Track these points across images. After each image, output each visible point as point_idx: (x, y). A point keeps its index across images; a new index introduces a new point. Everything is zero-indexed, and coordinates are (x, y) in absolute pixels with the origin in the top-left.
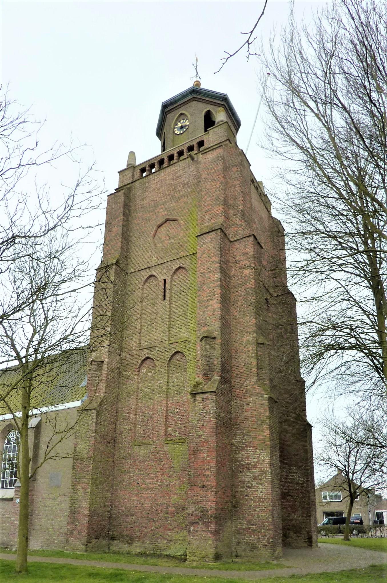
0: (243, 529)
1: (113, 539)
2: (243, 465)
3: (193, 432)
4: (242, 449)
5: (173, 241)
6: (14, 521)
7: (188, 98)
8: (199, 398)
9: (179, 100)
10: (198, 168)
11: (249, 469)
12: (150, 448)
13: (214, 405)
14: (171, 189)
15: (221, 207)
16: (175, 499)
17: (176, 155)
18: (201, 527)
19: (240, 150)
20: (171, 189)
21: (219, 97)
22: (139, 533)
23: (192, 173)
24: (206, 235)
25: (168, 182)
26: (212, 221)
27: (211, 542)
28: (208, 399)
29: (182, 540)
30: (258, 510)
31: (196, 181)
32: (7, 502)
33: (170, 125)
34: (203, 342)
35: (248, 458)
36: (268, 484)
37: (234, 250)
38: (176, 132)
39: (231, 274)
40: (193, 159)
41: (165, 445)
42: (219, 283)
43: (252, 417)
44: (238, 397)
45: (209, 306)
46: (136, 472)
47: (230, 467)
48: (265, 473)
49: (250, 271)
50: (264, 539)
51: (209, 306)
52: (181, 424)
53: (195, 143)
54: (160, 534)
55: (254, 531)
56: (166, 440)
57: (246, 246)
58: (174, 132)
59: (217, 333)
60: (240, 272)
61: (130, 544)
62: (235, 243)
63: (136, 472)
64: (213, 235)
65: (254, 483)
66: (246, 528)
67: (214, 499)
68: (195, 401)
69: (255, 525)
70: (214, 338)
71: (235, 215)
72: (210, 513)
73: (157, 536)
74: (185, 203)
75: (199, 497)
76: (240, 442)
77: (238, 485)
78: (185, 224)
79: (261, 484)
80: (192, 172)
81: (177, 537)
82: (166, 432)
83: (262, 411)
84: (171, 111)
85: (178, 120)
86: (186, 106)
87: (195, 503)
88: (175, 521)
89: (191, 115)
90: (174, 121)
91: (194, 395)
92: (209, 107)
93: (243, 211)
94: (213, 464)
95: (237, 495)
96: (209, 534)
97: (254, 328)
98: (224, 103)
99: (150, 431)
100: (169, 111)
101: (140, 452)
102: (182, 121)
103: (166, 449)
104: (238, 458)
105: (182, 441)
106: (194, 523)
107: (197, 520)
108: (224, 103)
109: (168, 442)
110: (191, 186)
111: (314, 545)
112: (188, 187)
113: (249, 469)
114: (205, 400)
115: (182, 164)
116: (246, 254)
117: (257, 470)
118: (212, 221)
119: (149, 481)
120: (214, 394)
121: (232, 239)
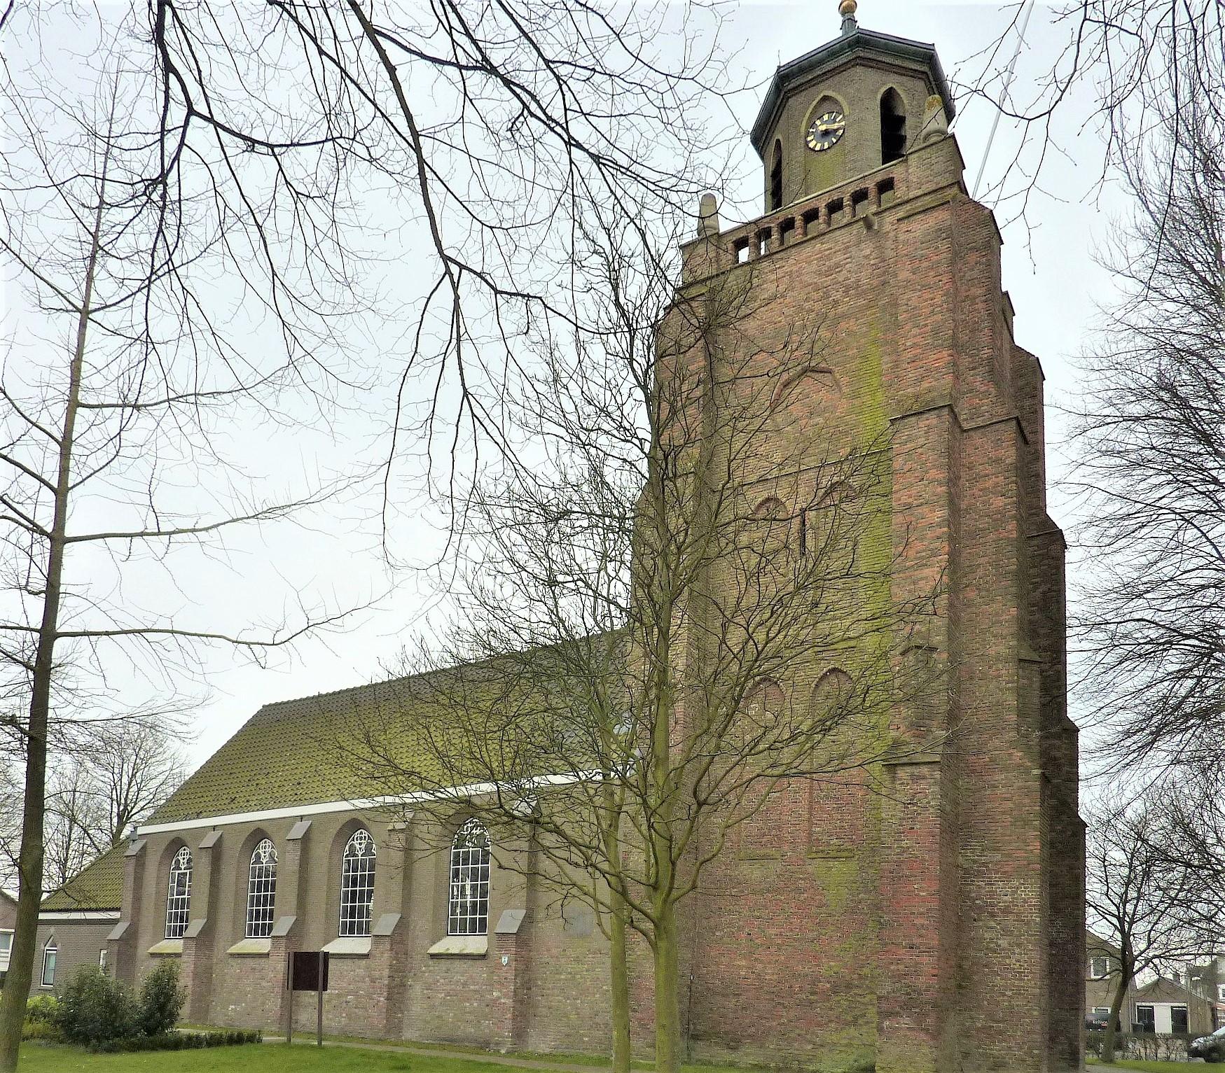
0: (978, 1030)
1: (695, 1037)
2: (980, 908)
3: (889, 841)
4: (979, 874)
5: (821, 420)
6: (499, 998)
7: (843, 59)
8: (903, 773)
9: (821, 62)
10: (880, 248)
11: (993, 915)
12: (776, 867)
13: (937, 789)
14: (815, 296)
15: (945, 353)
16: (830, 967)
17: (823, 211)
18: (905, 1021)
19: (986, 212)
20: (815, 296)
21: (915, 54)
22: (753, 1029)
23: (866, 262)
24: (913, 419)
25: (806, 278)
26: (925, 385)
27: (926, 1050)
28: (924, 778)
29: (846, 1046)
30: (1009, 993)
31: (875, 282)
32: (470, 962)
33: (798, 127)
34: (911, 657)
35: (992, 894)
36: (1034, 945)
37: (970, 450)
38: (811, 145)
39: (963, 506)
40: (869, 226)
41: (809, 861)
42: (946, 529)
43: (1004, 813)
44: (973, 771)
45: (922, 579)
46: (745, 912)
47: (961, 912)
48: (1028, 923)
49: (1007, 501)
50: (1021, 1048)
51: (922, 579)
52: (842, 820)
53: (871, 185)
54: (798, 1031)
55: (1001, 1033)
56: (809, 852)
57: (998, 443)
58: (807, 143)
59: (938, 639)
60: (984, 503)
61: (734, 1049)
62: (972, 433)
63: (745, 912)
64: (932, 419)
65: (1003, 943)
66: (984, 1028)
67: (935, 972)
68: (894, 779)
69: (1003, 1021)
70: (933, 649)
71: (974, 369)
72: (926, 997)
73: (792, 1035)
74: (850, 333)
75: (901, 967)
76: (975, 862)
77: (969, 945)
78: (850, 384)
79: (1019, 945)
80: (866, 257)
81: (834, 1038)
82: (810, 835)
83: (1027, 801)
84: (797, 90)
85: (817, 114)
86: (837, 78)
87: (894, 976)
88: (831, 1009)
89: (851, 104)
90: (808, 115)
91: (891, 767)
92: (892, 81)
93: (990, 359)
94: (934, 905)
95: (966, 964)
96: (923, 1036)
97: (1014, 629)
98: (925, 68)
99: (774, 832)
100: (794, 89)
101: (753, 872)
102: (826, 117)
103: (810, 869)
104: (970, 892)
105: (845, 854)
106: (890, 1014)
107: (898, 1009)
108: (925, 68)
109: (814, 855)
110: (864, 292)
111: (1081, 1066)
112: (858, 295)
113: (993, 915)
114: (916, 779)
115: (842, 237)
116: (998, 461)
117: (1011, 917)
118: (925, 385)
119: (772, 931)
120: (936, 767)
121: (966, 426)
